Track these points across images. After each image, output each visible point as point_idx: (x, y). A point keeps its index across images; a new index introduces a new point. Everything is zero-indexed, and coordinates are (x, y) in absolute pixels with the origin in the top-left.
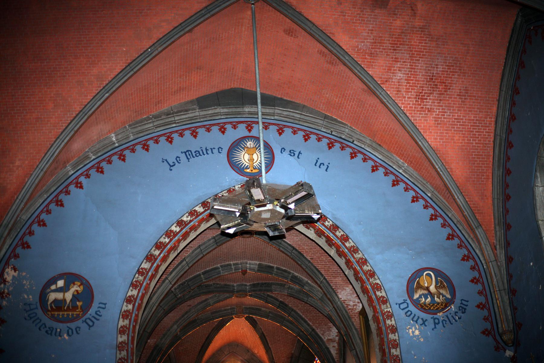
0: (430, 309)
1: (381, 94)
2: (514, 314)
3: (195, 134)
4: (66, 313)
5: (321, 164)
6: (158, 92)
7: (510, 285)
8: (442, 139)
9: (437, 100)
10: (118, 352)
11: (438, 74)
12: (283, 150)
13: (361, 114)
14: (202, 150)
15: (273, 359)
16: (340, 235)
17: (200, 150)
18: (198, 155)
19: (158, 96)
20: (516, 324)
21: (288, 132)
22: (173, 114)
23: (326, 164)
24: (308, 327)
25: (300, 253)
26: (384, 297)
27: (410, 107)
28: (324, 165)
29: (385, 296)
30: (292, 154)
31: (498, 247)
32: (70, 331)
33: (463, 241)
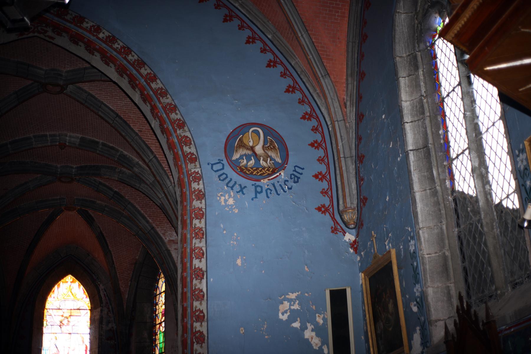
0: (252, 173)
2: (360, 187)
7: (358, 150)
15: (113, 263)
16: (146, 73)
20: (361, 199)
24: (147, 225)
25: (125, 122)
26: (193, 154)
29: (195, 153)
31: (348, 103)
33: (306, 96)
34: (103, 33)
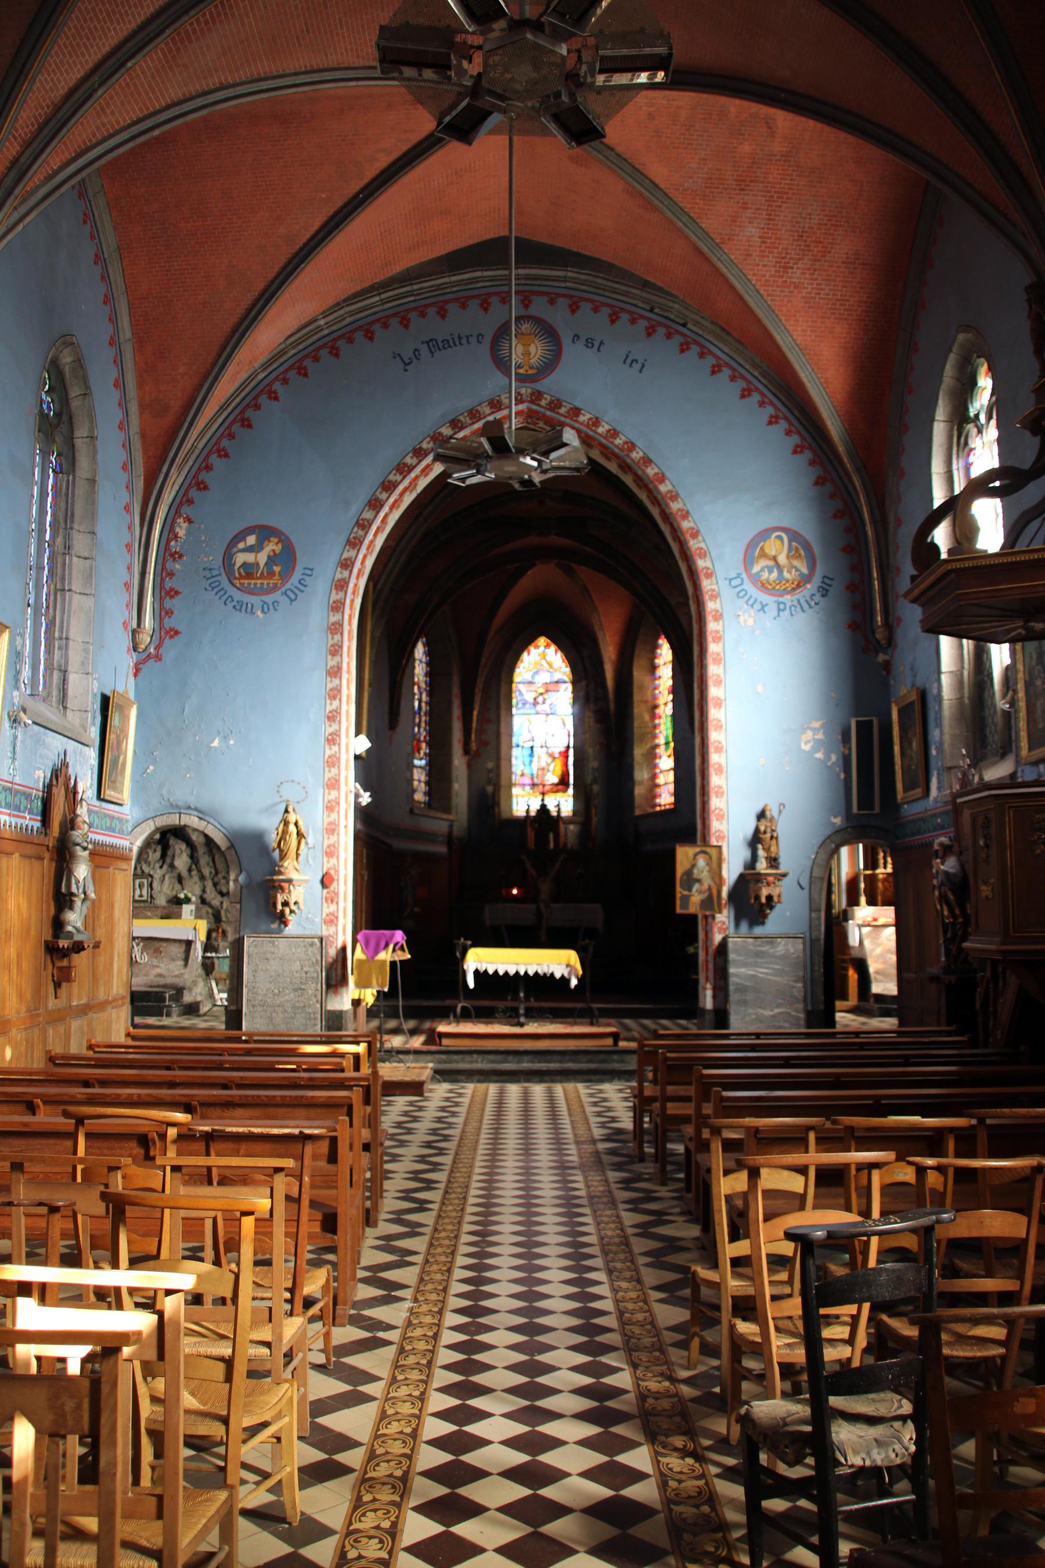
1: (719, 259)
3: (442, 313)
4: (259, 582)
8: (815, 332)
9: (809, 269)
10: (330, 636)
11: (812, 228)
12: (576, 337)
17: (449, 338)
21: (586, 307)
22: (410, 280)
23: (641, 361)
26: (708, 569)
27: (767, 281)
32: (266, 607)
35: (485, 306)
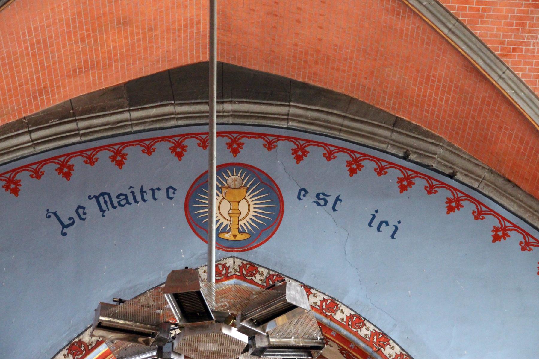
3: (119, 159)
5: (382, 223)
6: (37, 72)
12: (303, 192)
13: (467, 117)
14: (133, 192)
18: (123, 202)
19: (38, 78)
21: (315, 154)
22: (74, 115)
23: (392, 223)
28: (387, 224)
30: (322, 202)
34: (342, 311)
35: (179, 151)
